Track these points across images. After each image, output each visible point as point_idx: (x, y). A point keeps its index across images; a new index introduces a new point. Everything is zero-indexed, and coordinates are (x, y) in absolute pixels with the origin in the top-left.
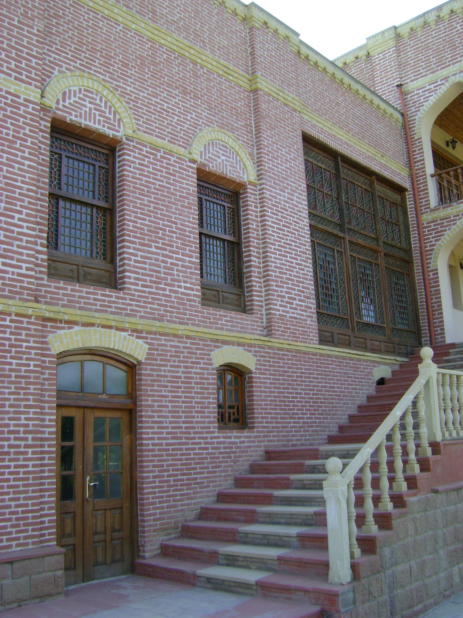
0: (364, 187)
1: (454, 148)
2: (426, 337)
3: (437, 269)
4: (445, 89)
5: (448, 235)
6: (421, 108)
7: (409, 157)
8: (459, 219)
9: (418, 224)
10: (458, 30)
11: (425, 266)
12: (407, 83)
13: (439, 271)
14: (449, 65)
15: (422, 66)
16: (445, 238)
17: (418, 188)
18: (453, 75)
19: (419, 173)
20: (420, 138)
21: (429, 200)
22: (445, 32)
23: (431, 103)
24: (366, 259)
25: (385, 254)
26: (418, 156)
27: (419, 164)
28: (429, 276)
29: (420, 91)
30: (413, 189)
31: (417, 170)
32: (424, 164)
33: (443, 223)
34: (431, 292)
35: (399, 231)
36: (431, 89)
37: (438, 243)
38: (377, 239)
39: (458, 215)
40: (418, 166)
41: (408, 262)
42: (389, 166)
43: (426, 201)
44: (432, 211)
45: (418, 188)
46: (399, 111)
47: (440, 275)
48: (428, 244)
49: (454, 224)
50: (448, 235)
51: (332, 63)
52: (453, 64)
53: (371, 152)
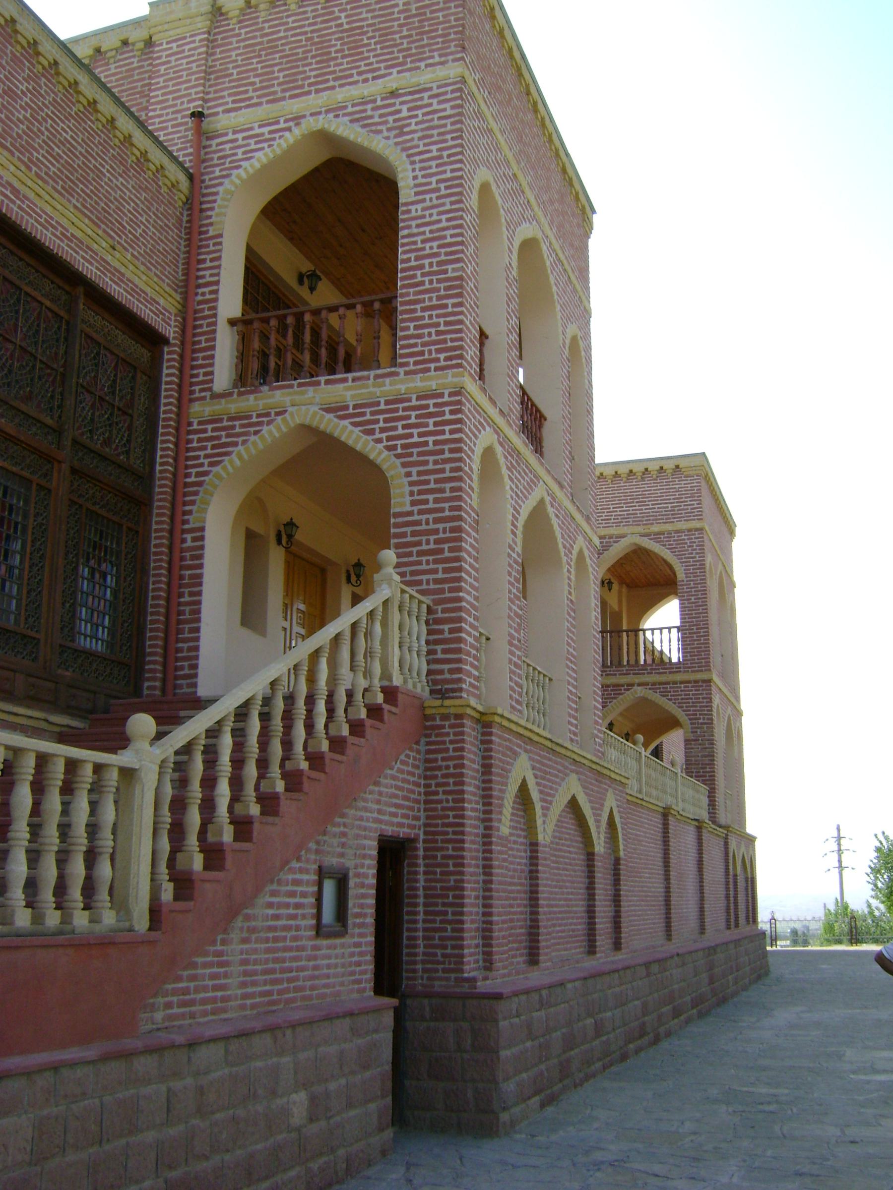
0: (48, 303)
1: (312, 289)
2: (154, 679)
3: (202, 529)
4: (291, 141)
5: (240, 457)
6: (235, 172)
7: (187, 274)
8: (269, 423)
9: (178, 422)
10: (341, 25)
11: (179, 518)
12: (217, 114)
13: (208, 534)
14: (308, 93)
15: (253, 84)
16: (231, 462)
17: (194, 343)
18: (311, 115)
19: (203, 310)
20: (221, 236)
21: (212, 373)
22: (315, 24)
23: (258, 165)
24: (14, 469)
25: (74, 471)
26: (208, 273)
27: (206, 290)
28: (184, 541)
29: (240, 136)
30: (183, 343)
31: (200, 303)
32: (216, 292)
33: (234, 427)
34: (181, 577)
35: (130, 428)
36: (263, 134)
37: (214, 469)
38: (58, 432)
39: (268, 415)
40: (203, 294)
41: (139, 503)
42: (128, 274)
43: (205, 374)
44: (216, 396)
45: (194, 343)
46: (186, 170)
47: (208, 543)
48: (194, 471)
49: (256, 433)
50: (240, 457)
51: (63, 46)
52: (318, 91)
53: (82, 228)
